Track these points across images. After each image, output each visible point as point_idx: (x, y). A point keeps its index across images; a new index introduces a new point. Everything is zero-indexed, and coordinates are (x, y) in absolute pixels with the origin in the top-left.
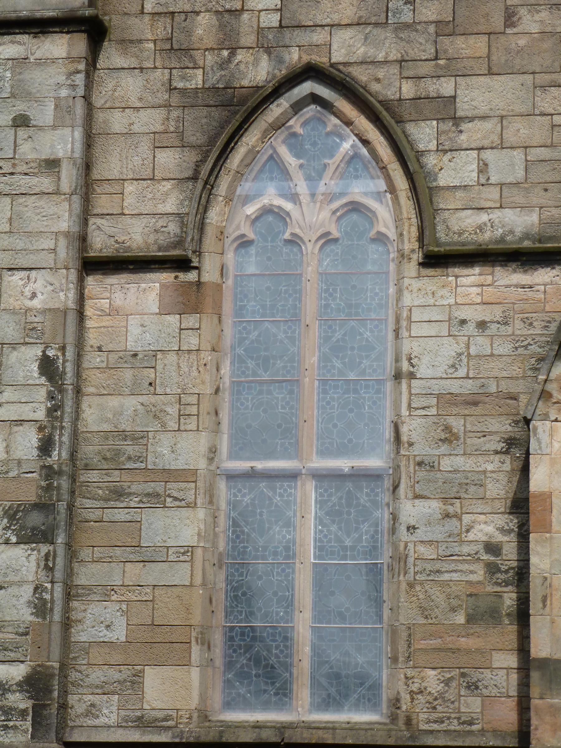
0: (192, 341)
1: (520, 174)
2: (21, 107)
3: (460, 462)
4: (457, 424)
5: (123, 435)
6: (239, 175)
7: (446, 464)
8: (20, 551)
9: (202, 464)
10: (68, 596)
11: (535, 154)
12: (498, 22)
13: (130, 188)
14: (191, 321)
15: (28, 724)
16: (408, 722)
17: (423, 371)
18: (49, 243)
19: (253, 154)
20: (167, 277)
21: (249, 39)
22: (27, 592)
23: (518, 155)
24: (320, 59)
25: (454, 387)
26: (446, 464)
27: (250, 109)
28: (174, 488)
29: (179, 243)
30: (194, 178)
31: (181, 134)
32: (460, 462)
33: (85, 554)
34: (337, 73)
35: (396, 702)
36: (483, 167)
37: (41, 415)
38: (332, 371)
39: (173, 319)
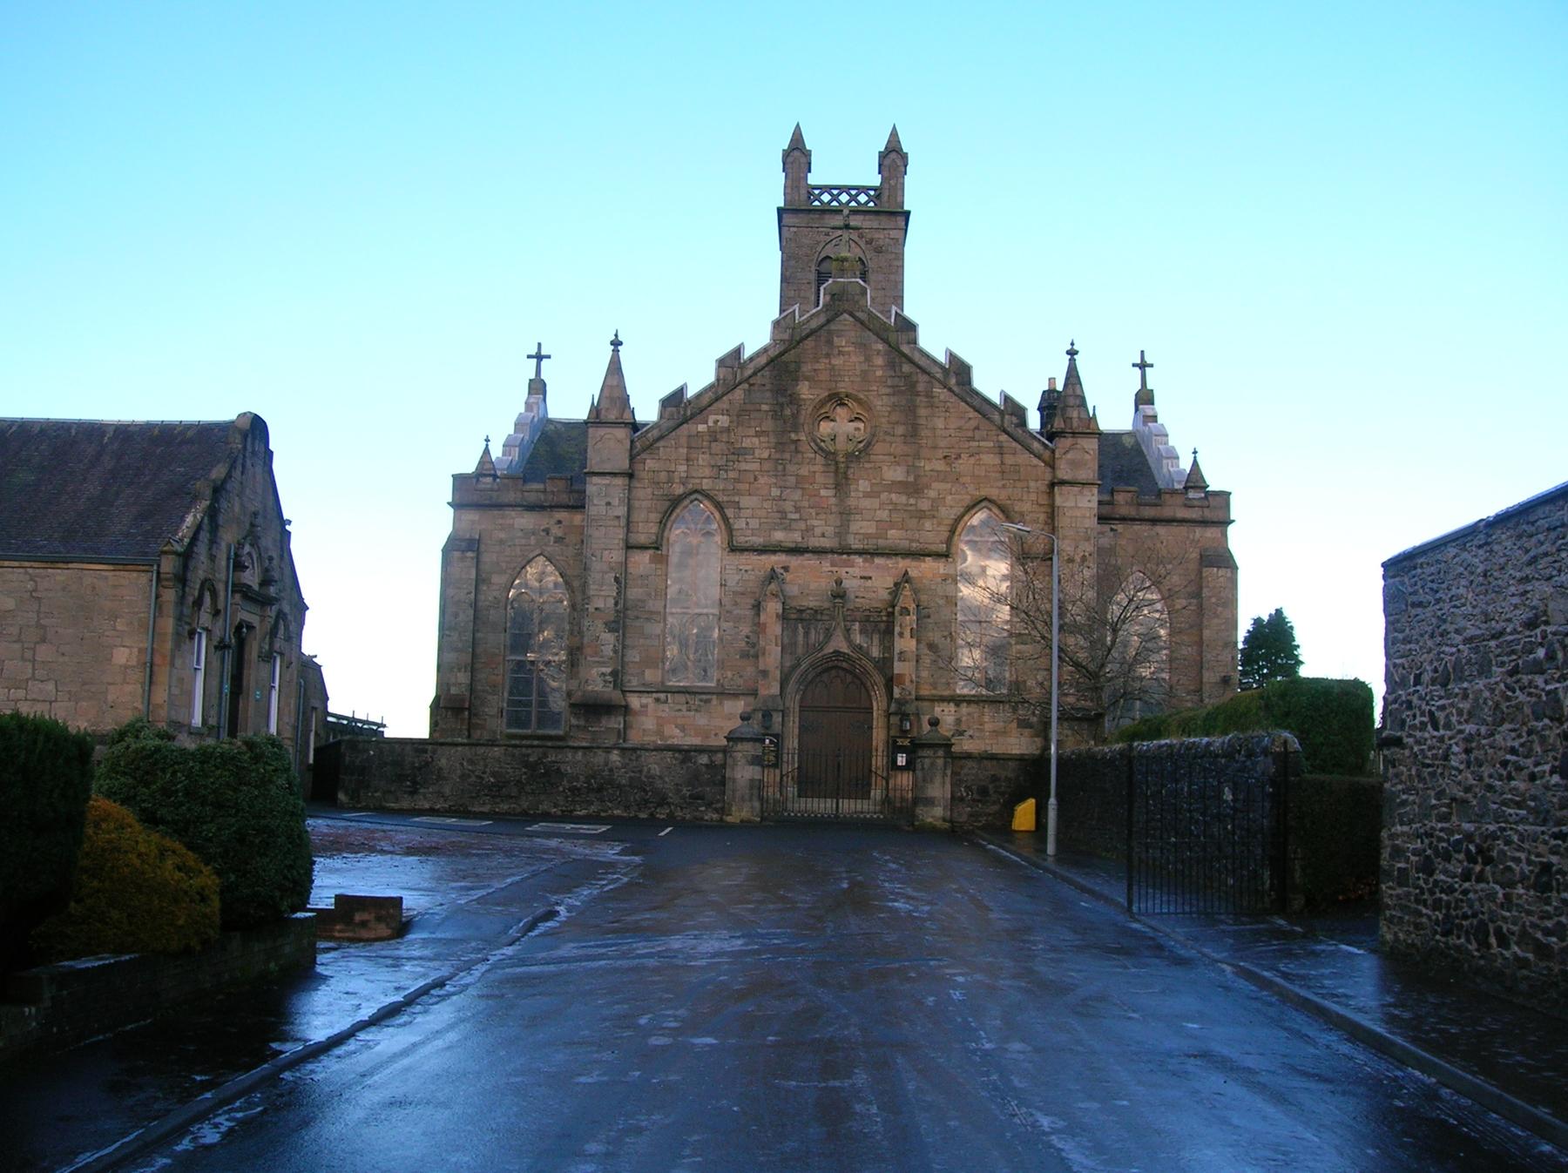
0: (659, 572)
1: (758, 526)
2: (608, 499)
3: (739, 611)
4: (738, 600)
5: (639, 600)
6: (674, 522)
7: (735, 612)
8: (609, 635)
9: (662, 610)
10: (623, 648)
11: (762, 520)
12: (752, 480)
13: (640, 524)
14: (658, 566)
15: (612, 685)
16: (722, 686)
17: (728, 584)
18: (616, 541)
19: (678, 515)
20: (651, 552)
21: (678, 481)
22: (611, 646)
23: (757, 521)
24: (699, 488)
25: (738, 589)
26: (735, 612)
27: (557, 831)
28: (654, 616)
29: (656, 542)
30: (661, 522)
31: (656, 509)
32: (739, 611)
33: (627, 635)
34: (384, 953)
35: (718, 680)
36: (747, 524)
37: (615, 594)
38: (1437, 890)
39: (653, 565)
